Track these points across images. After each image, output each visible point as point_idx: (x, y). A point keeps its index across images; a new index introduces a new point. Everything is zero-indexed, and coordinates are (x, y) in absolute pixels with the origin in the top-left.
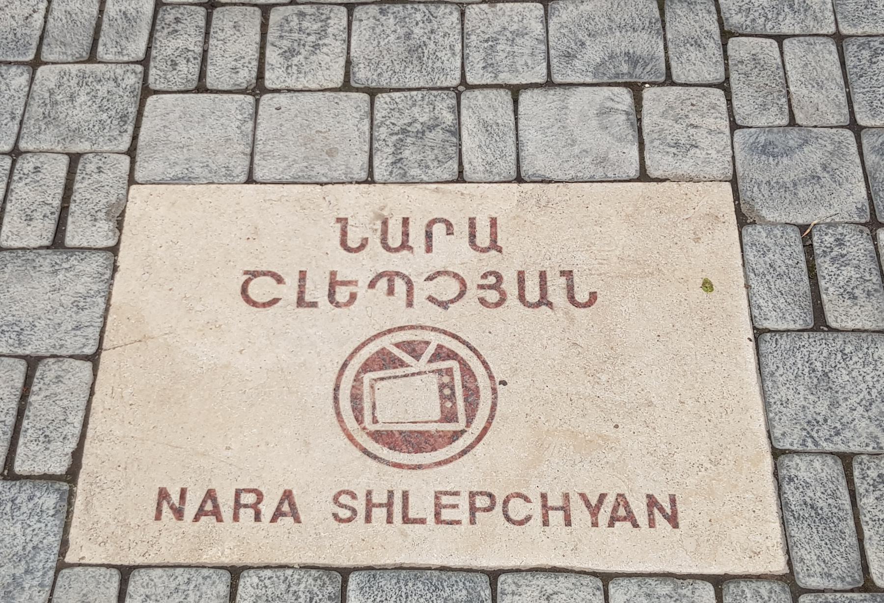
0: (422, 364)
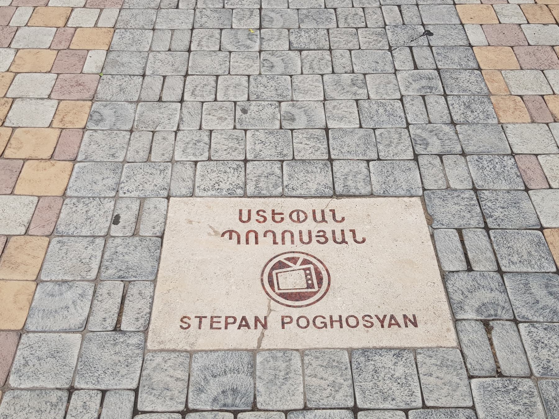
0: (298, 266)
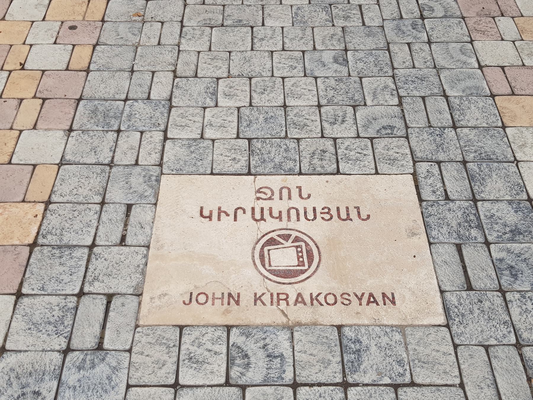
0: (289, 243)
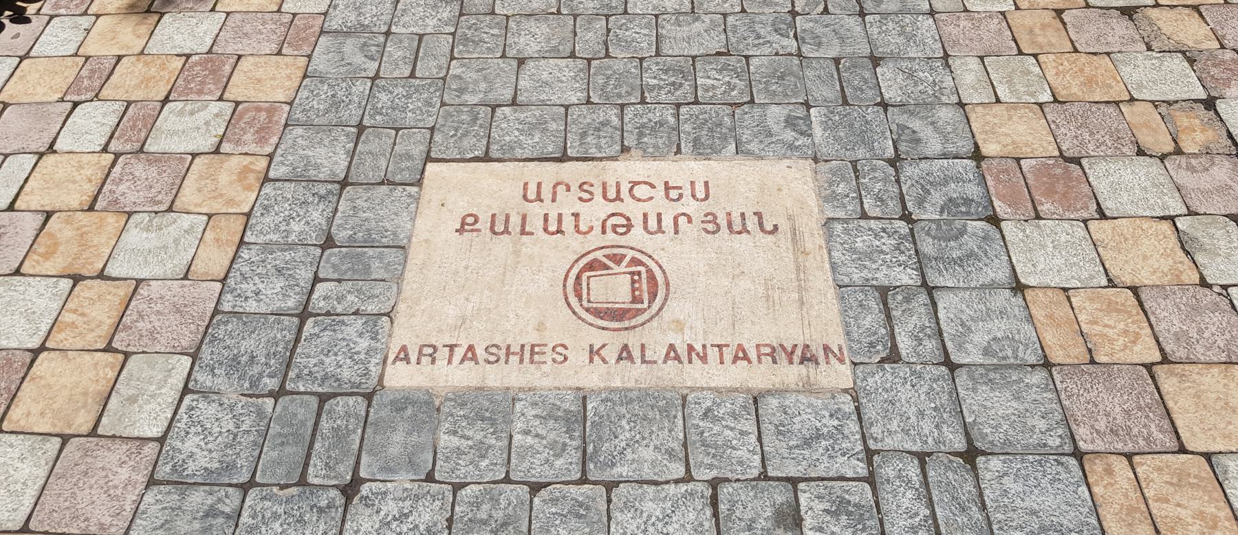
0: (623, 268)
